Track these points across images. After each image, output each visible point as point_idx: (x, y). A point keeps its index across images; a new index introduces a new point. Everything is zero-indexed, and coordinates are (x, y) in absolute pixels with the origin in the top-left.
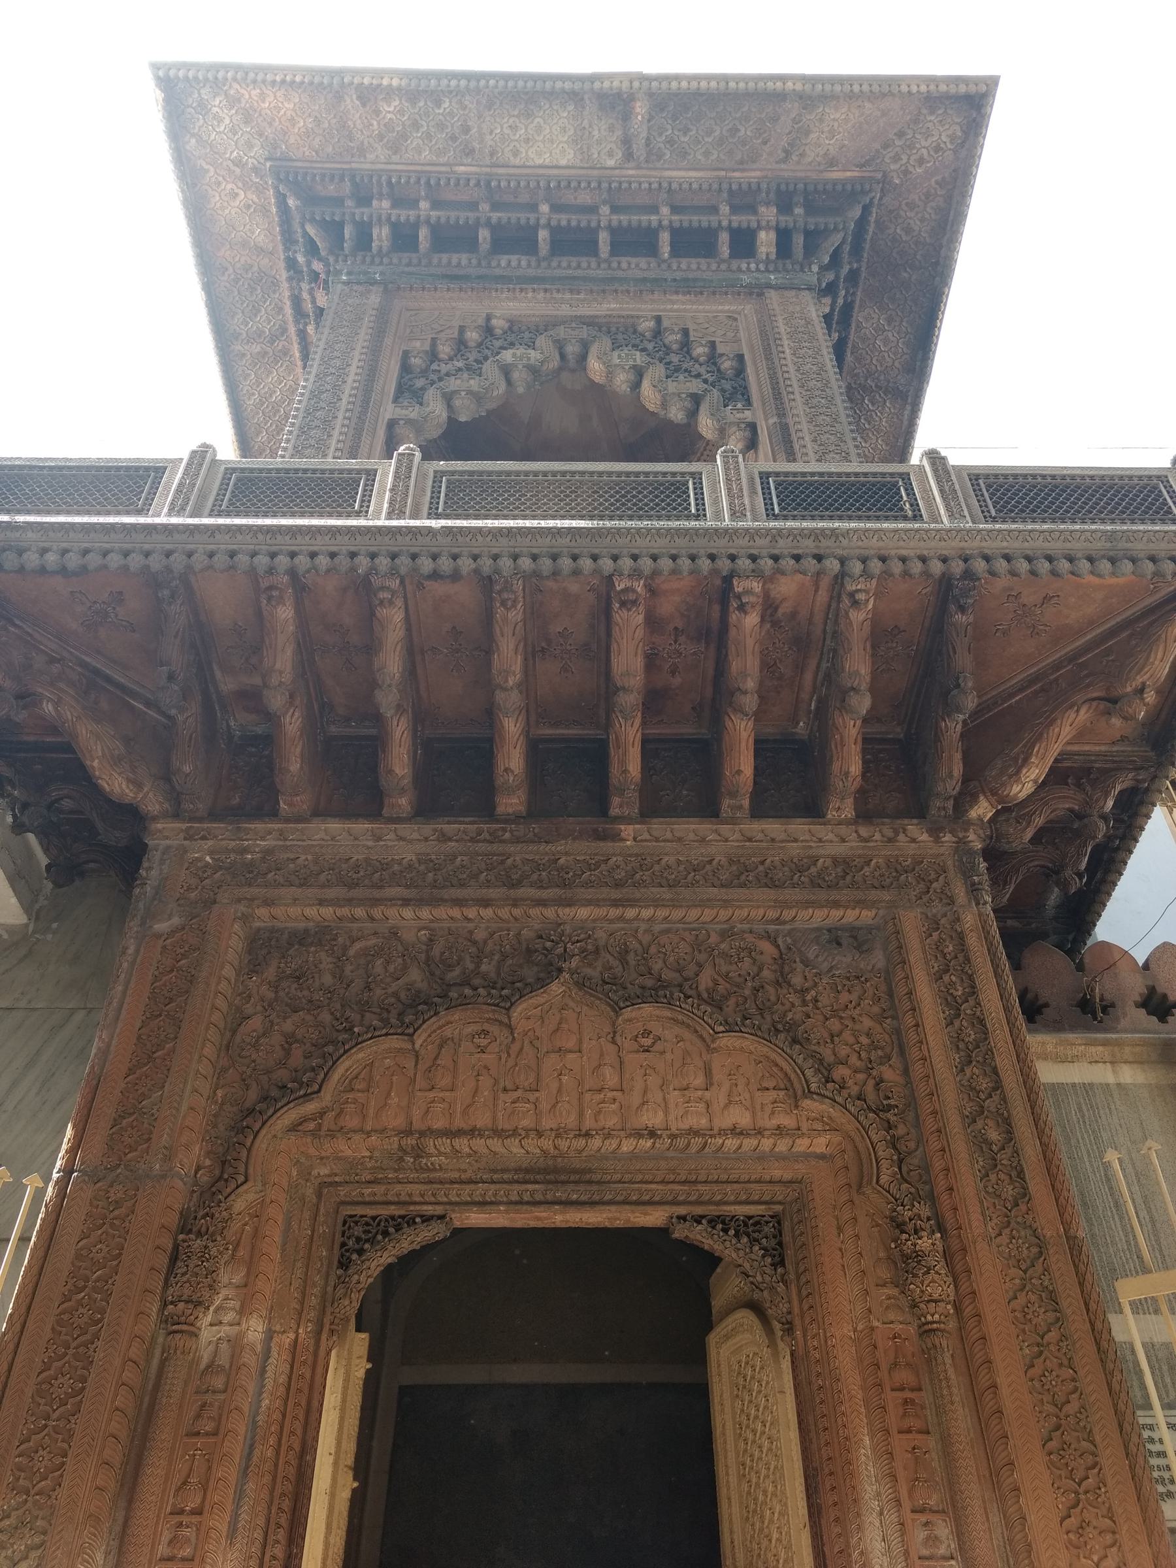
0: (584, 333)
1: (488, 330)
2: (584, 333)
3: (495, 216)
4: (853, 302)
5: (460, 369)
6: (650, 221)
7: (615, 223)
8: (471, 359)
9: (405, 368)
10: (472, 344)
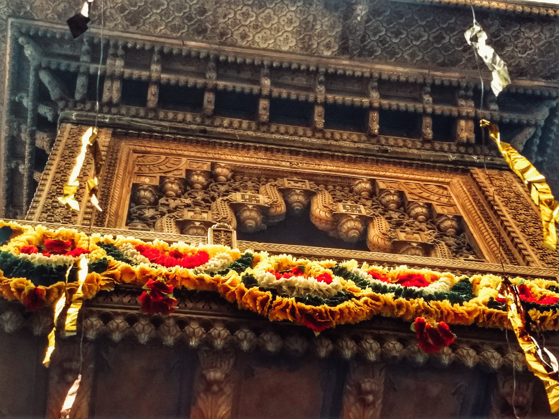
0: (308, 185)
1: (212, 176)
2: (308, 185)
3: (127, 72)
6: (187, 82)
8: (199, 198)
9: (135, 199)
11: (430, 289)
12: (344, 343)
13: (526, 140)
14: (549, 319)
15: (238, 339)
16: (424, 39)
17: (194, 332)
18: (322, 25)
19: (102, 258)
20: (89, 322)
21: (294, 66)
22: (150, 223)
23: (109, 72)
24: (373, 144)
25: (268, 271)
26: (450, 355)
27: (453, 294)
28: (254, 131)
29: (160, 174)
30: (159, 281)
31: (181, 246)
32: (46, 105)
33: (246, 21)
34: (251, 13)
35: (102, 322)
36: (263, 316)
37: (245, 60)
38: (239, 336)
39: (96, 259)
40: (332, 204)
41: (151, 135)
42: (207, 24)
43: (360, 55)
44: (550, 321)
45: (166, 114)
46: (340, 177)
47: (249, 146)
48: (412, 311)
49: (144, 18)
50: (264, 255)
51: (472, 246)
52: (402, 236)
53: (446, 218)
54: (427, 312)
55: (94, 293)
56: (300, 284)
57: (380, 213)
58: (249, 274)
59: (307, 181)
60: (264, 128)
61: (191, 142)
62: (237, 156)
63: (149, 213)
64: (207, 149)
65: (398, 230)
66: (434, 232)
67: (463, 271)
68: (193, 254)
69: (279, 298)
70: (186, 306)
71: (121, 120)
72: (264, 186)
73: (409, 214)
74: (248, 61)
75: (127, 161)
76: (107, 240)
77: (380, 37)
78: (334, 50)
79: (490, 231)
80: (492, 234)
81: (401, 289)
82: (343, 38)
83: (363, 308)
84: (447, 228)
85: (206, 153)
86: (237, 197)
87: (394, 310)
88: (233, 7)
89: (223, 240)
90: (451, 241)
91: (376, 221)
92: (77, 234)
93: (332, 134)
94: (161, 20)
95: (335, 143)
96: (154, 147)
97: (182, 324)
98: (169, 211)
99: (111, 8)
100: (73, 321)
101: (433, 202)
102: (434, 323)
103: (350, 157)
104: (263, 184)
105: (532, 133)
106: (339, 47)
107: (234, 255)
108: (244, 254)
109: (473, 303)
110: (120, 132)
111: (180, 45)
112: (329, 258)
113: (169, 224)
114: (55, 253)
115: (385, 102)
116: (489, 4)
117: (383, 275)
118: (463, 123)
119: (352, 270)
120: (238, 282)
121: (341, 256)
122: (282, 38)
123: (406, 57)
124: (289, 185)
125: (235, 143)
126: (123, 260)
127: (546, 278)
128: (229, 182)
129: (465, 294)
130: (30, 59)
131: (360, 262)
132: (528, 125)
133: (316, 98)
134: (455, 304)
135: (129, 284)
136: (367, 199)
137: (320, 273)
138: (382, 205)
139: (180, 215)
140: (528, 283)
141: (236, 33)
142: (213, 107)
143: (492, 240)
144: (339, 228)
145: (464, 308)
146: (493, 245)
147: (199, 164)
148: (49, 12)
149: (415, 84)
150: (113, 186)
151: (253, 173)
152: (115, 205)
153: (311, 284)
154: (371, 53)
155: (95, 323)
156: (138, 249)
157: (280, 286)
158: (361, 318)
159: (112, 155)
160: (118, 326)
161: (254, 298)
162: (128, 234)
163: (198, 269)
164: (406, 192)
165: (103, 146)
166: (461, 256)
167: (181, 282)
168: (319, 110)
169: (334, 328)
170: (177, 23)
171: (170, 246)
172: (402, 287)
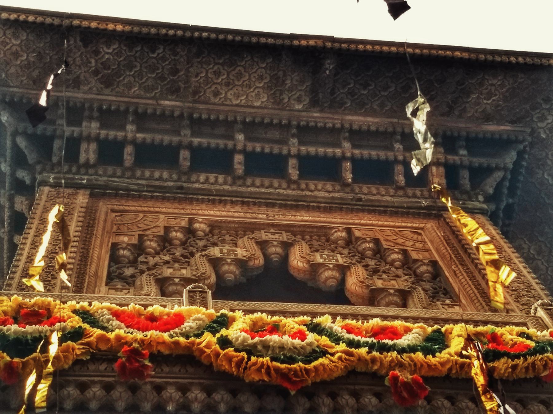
0: (285, 237)
1: (190, 231)
2: (285, 237)
6: (162, 140)
8: (178, 254)
9: (114, 259)
10: (177, 242)
11: (404, 341)
12: (321, 401)
13: (495, 183)
14: (521, 366)
15: (215, 401)
16: (391, 90)
17: (171, 397)
18: (292, 80)
19: (77, 326)
20: (66, 392)
21: (266, 121)
22: (129, 283)
23: (85, 134)
24: (348, 193)
25: (243, 331)
26: (425, 407)
27: (425, 346)
28: (230, 185)
29: (138, 233)
30: (134, 347)
31: (156, 309)
32: (24, 169)
33: (217, 79)
34: (222, 71)
35: (78, 392)
36: (239, 377)
37: (218, 118)
38: (216, 398)
39: (72, 327)
40: (309, 254)
41: (128, 194)
42: (180, 83)
43: (330, 107)
44: (521, 369)
45: (143, 173)
46: (316, 227)
47: (226, 200)
48: (386, 366)
49: (118, 80)
50: (238, 314)
51: (448, 290)
52: (379, 284)
53: (422, 263)
54: (401, 365)
55: (71, 362)
56: (275, 342)
57: (357, 261)
58: (224, 335)
59: (283, 232)
60: (240, 182)
61: (168, 199)
62: (214, 210)
63: (128, 272)
64: (184, 205)
65: (375, 278)
66: (410, 278)
67: (436, 321)
68: (169, 317)
69: (253, 359)
70: (162, 370)
71: (98, 180)
72: (242, 239)
73: (385, 261)
74: (221, 117)
75: (105, 221)
76: (82, 307)
77: (349, 89)
78: (305, 103)
79: (465, 274)
80: (467, 278)
81: (375, 343)
83: (337, 365)
84: (422, 273)
85: (183, 209)
86: (215, 252)
87: (368, 364)
88: (204, 66)
89: (198, 301)
90: (428, 286)
91: (353, 270)
92: (53, 303)
93: (307, 185)
94: (135, 81)
95: (310, 193)
96: (132, 206)
97: (159, 389)
98: (149, 269)
99: (85, 72)
100: (43, 397)
101: (408, 248)
102: (406, 376)
103: (325, 206)
104: (241, 238)
105: (502, 176)
106: (310, 100)
107: (209, 316)
108: (219, 314)
109: (445, 354)
110: (98, 193)
111: (153, 105)
112: (303, 314)
113: (148, 281)
114: (30, 324)
115: (357, 152)
116: (453, 53)
117: (357, 328)
119: (326, 326)
120: (213, 344)
121: (315, 311)
122: (253, 94)
123: (375, 107)
124: (267, 237)
125: (212, 198)
126: (99, 327)
127: (517, 324)
128: (207, 237)
129: (438, 344)
130: (6, 125)
131: (334, 316)
132: (498, 168)
133: (289, 151)
134: (428, 356)
135: (105, 351)
136: (344, 248)
137: (295, 330)
138: (359, 253)
139: (160, 272)
140: (499, 330)
141: (208, 91)
142: (189, 164)
143: (468, 283)
144: (317, 277)
145: (437, 359)
146: (469, 289)
147: (177, 221)
148: (24, 78)
149: (385, 133)
150: (92, 247)
151: (230, 227)
152: (94, 266)
153: (286, 343)
155: (72, 392)
156: (117, 312)
157: (255, 345)
158: (336, 375)
159: (90, 216)
160: (95, 393)
161: (229, 359)
162: (104, 299)
163: (174, 332)
164: (382, 239)
165: (82, 207)
166: (438, 300)
167: (157, 346)
168: (292, 162)
169: (310, 385)
170: (150, 84)
171: (145, 309)
172: (375, 341)
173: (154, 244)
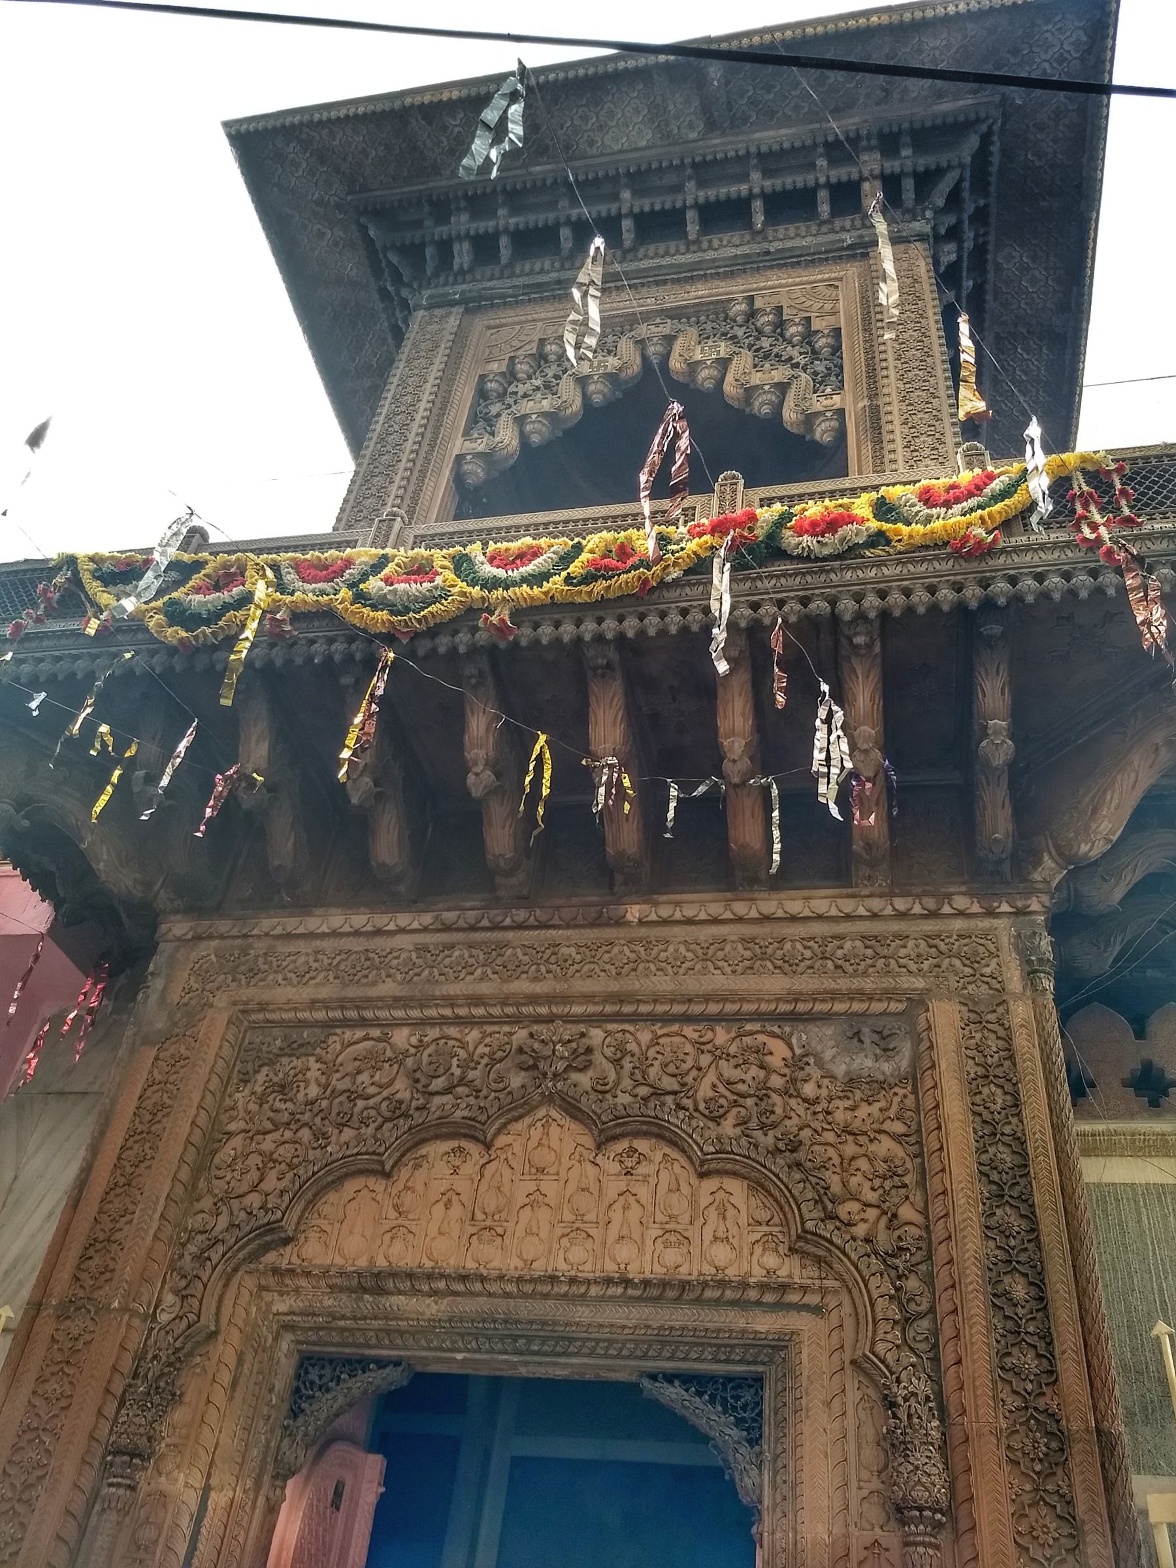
0: (666, 328)
4: (985, 243)
5: (538, 388)
6: (739, 192)
7: (701, 200)
8: (550, 374)
9: (482, 394)
82: (706, 110)
118: (866, 186)
132: (950, 167)
154: (745, 119)
173: (525, 367)
